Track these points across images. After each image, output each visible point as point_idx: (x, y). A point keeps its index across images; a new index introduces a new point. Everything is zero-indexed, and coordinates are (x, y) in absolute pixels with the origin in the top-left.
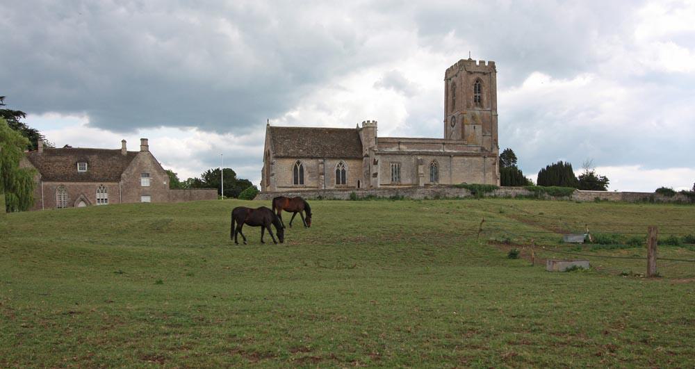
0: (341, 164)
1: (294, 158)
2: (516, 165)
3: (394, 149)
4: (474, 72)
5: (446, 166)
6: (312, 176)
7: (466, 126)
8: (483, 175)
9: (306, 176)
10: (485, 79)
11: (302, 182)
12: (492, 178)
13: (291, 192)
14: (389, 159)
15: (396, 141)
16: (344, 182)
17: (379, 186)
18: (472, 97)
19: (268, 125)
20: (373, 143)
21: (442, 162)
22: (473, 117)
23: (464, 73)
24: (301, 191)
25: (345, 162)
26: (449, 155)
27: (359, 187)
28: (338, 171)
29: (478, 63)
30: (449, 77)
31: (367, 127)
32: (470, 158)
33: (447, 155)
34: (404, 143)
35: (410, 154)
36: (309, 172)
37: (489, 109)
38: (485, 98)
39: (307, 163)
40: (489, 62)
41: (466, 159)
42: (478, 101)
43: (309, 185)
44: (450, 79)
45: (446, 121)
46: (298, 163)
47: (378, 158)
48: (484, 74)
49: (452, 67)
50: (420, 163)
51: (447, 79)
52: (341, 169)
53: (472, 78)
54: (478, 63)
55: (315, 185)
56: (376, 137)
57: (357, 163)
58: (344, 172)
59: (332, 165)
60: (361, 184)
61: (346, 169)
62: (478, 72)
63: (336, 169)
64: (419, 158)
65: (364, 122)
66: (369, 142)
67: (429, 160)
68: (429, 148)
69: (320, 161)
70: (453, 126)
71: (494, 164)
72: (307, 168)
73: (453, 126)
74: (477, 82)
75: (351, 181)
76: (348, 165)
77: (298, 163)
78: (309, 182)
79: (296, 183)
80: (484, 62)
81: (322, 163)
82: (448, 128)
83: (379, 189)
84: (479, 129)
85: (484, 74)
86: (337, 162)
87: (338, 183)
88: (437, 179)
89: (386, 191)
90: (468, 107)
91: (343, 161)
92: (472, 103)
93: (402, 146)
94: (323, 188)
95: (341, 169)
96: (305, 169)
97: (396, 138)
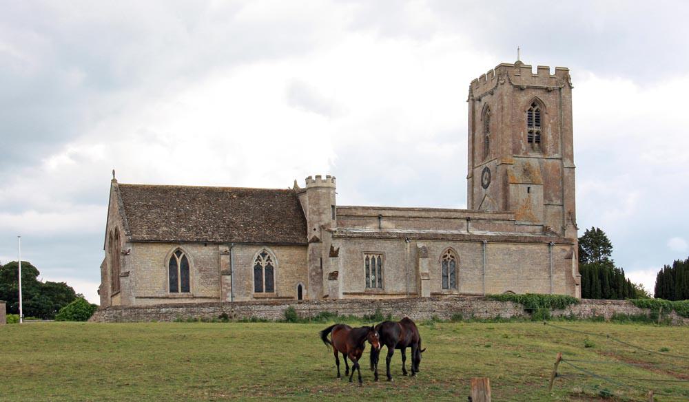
0: (264, 254)
1: (169, 243)
2: (610, 259)
3: (370, 229)
4: (528, 88)
5: (474, 261)
6: (205, 277)
7: (512, 187)
8: (547, 276)
9: (195, 277)
10: (549, 101)
11: (186, 288)
12: (563, 283)
13: (166, 306)
14: (361, 246)
15: (374, 213)
16: (270, 288)
17: (341, 297)
18: (524, 134)
19: (114, 181)
20: (327, 218)
21: (465, 254)
22: (525, 170)
23: (507, 88)
24: (186, 305)
25: (270, 251)
26: (480, 240)
27: (300, 296)
28: (258, 269)
29: (535, 71)
30: (476, 96)
31: (317, 188)
32: (521, 246)
33: (475, 241)
34: (389, 218)
35: (401, 237)
36: (200, 270)
37: (556, 156)
38: (549, 135)
39: (194, 253)
40: (539, 68)
41: (513, 247)
42: (536, 141)
43: (284, 295)
44: (480, 100)
45: (471, 177)
46: (178, 252)
47: (337, 244)
48: (548, 91)
49: (483, 77)
50: (421, 254)
51: (473, 100)
52: (264, 264)
53: (524, 99)
54: (535, 71)
55: (213, 293)
56: (333, 207)
57: (296, 253)
58: (270, 269)
59: (247, 257)
60: (304, 292)
61: (274, 264)
62: (536, 88)
63: (254, 264)
64: (420, 245)
65: (310, 178)
66: (320, 214)
67: (439, 248)
68: (438, 227)
69: (223, 248)
70: (486, 187)
71: (570, 257)
72: (196, 262)
73: (486, 187)
74: (534, 105)
75: (284, 286)
76: (279, 258)
77: (178, 252)
78: (199, 286)
79: (174, 289)
80: (547, 69)
81: (226, 253)
82: (476, 190)
83: (342, 302)
84: (538, 192)
85: (548, 91)
86: (256, 252)
87: (259, 289)
88: (455, 284)
89: (356, 305)
90: (516, 151)
91: (269, 250)
92: (524, 145)
93: (384, 223)
94: (229, 299)
95: (264, 264)
96: (191, 265)
97: (374, 208)
